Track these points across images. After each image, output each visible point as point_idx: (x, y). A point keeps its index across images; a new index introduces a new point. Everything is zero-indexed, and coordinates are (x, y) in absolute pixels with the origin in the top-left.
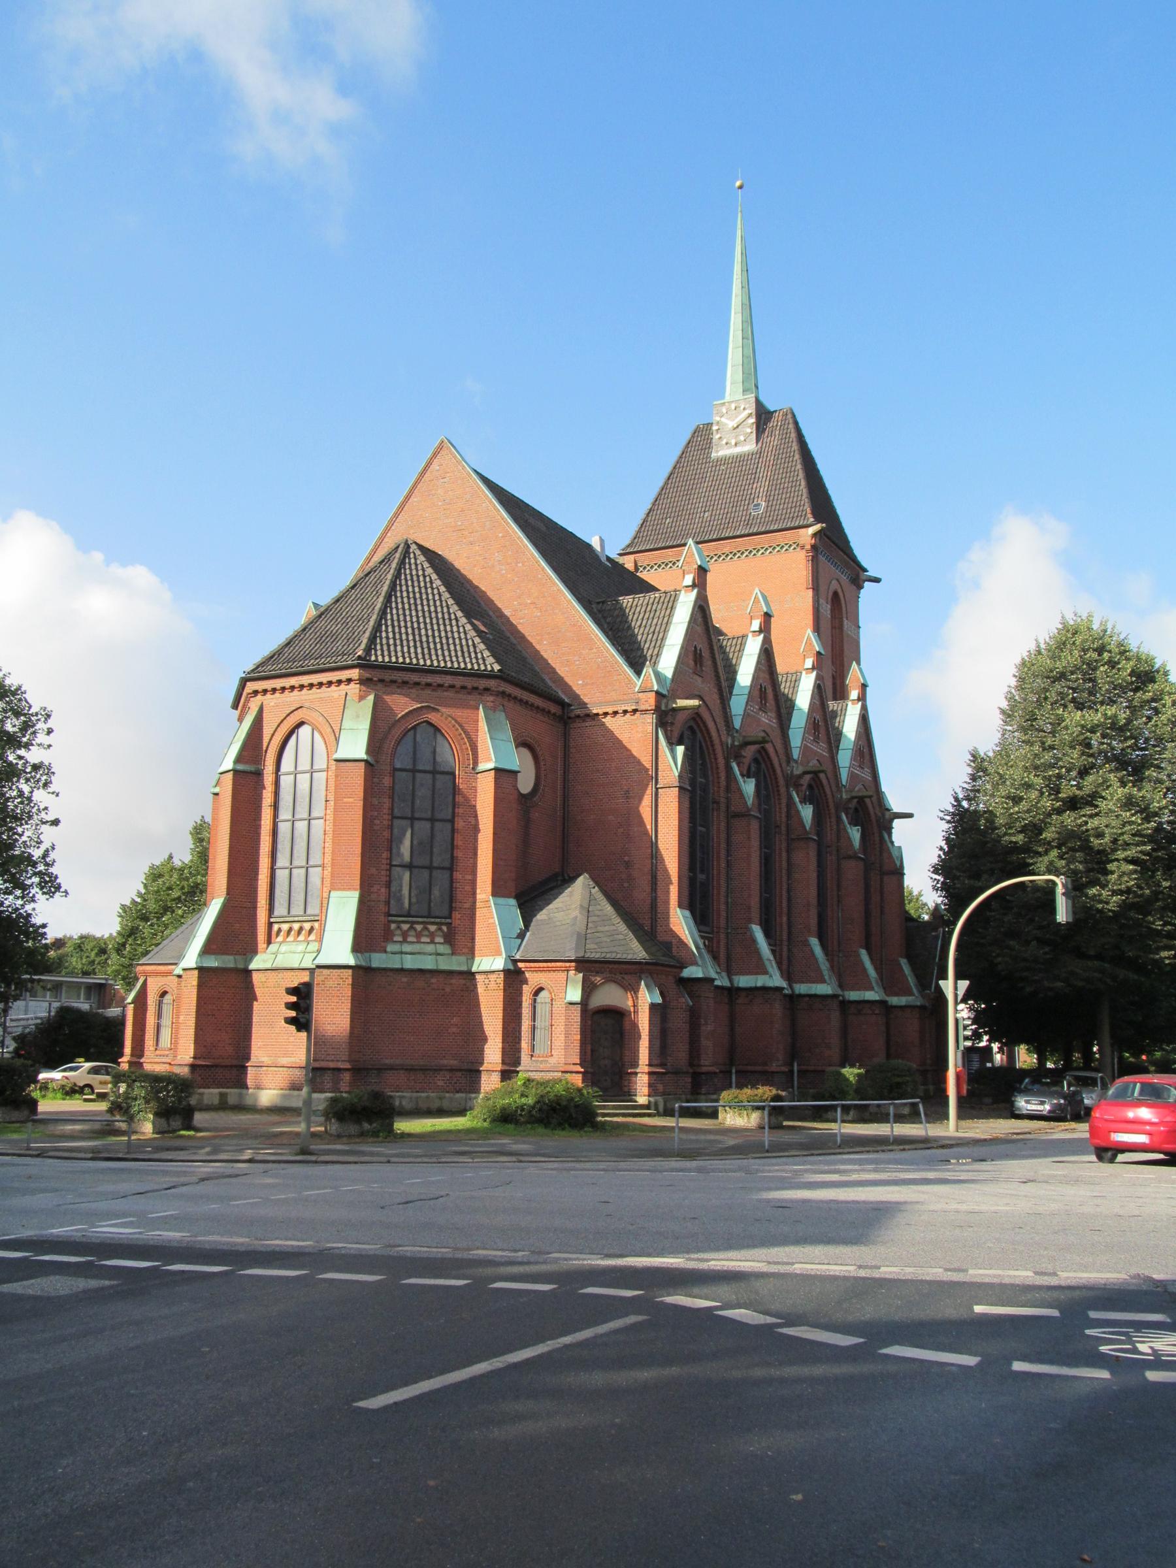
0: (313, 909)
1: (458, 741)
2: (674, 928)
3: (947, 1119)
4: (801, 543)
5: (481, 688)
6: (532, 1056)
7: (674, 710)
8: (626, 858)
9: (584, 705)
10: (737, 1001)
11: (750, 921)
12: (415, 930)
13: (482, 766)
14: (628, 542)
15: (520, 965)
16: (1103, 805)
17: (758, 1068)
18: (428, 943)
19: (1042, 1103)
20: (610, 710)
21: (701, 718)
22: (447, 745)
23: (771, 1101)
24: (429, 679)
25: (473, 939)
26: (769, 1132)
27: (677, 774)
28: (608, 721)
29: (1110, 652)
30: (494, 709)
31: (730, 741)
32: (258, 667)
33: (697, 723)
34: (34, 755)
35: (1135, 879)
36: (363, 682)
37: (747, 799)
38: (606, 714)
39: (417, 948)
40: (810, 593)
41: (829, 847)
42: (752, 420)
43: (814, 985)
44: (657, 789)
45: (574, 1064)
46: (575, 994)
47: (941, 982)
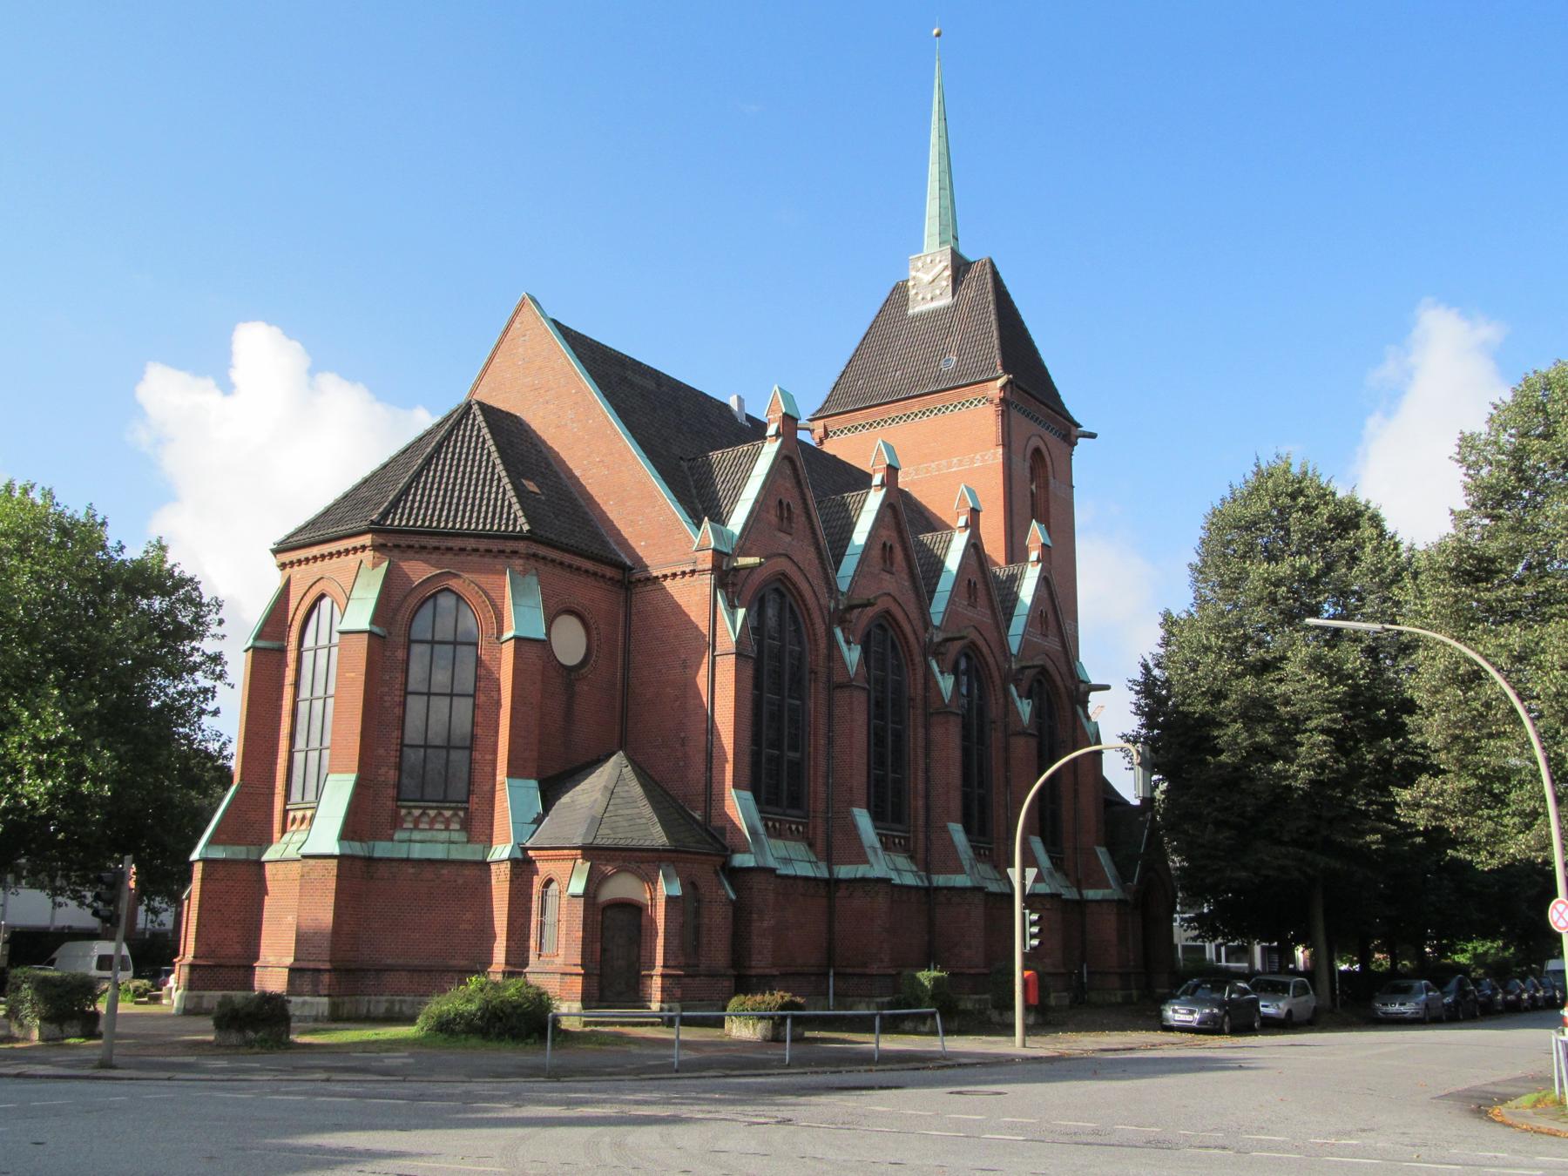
0: (310, 796)
1: (482, 609)
2: (728, 812)
4: (990, 397)
5: (417, 546)
6: (540, 955)
7: (735, 569)
8: (682, 735)
9: (645, 568)
10: (838, 894)
11: (851, 803)
12: (428, 815)
14: (819, 406)
15: (531, 853)
16: (1289, 668)
17: (858, 970)
18: (441, 830)
19: (1191, 1012)
20: (669, 572)
21: (789, 579)
22: (472, 615)
23: (778, 1009)
24: (451, 543)
25: (492, 825)
26: (790, 1045)
27: (734, 640)
28: (668, 584)
29: (1307, 496)
30: (525, 573)
31: (832, 605)
32: (288, 538)
33: (783, 583)
34: (208, 646)
35: (1327, 751)
37: (850, 668)
38: (665, 577)
39: (428, 835)
40: (1000, 450)
41: (994, 722)
42: (948, 273)
43: (953, 877)
44: (714, 657)
45: (575, 965)
46: (578, 886)
47: (1009, 870)
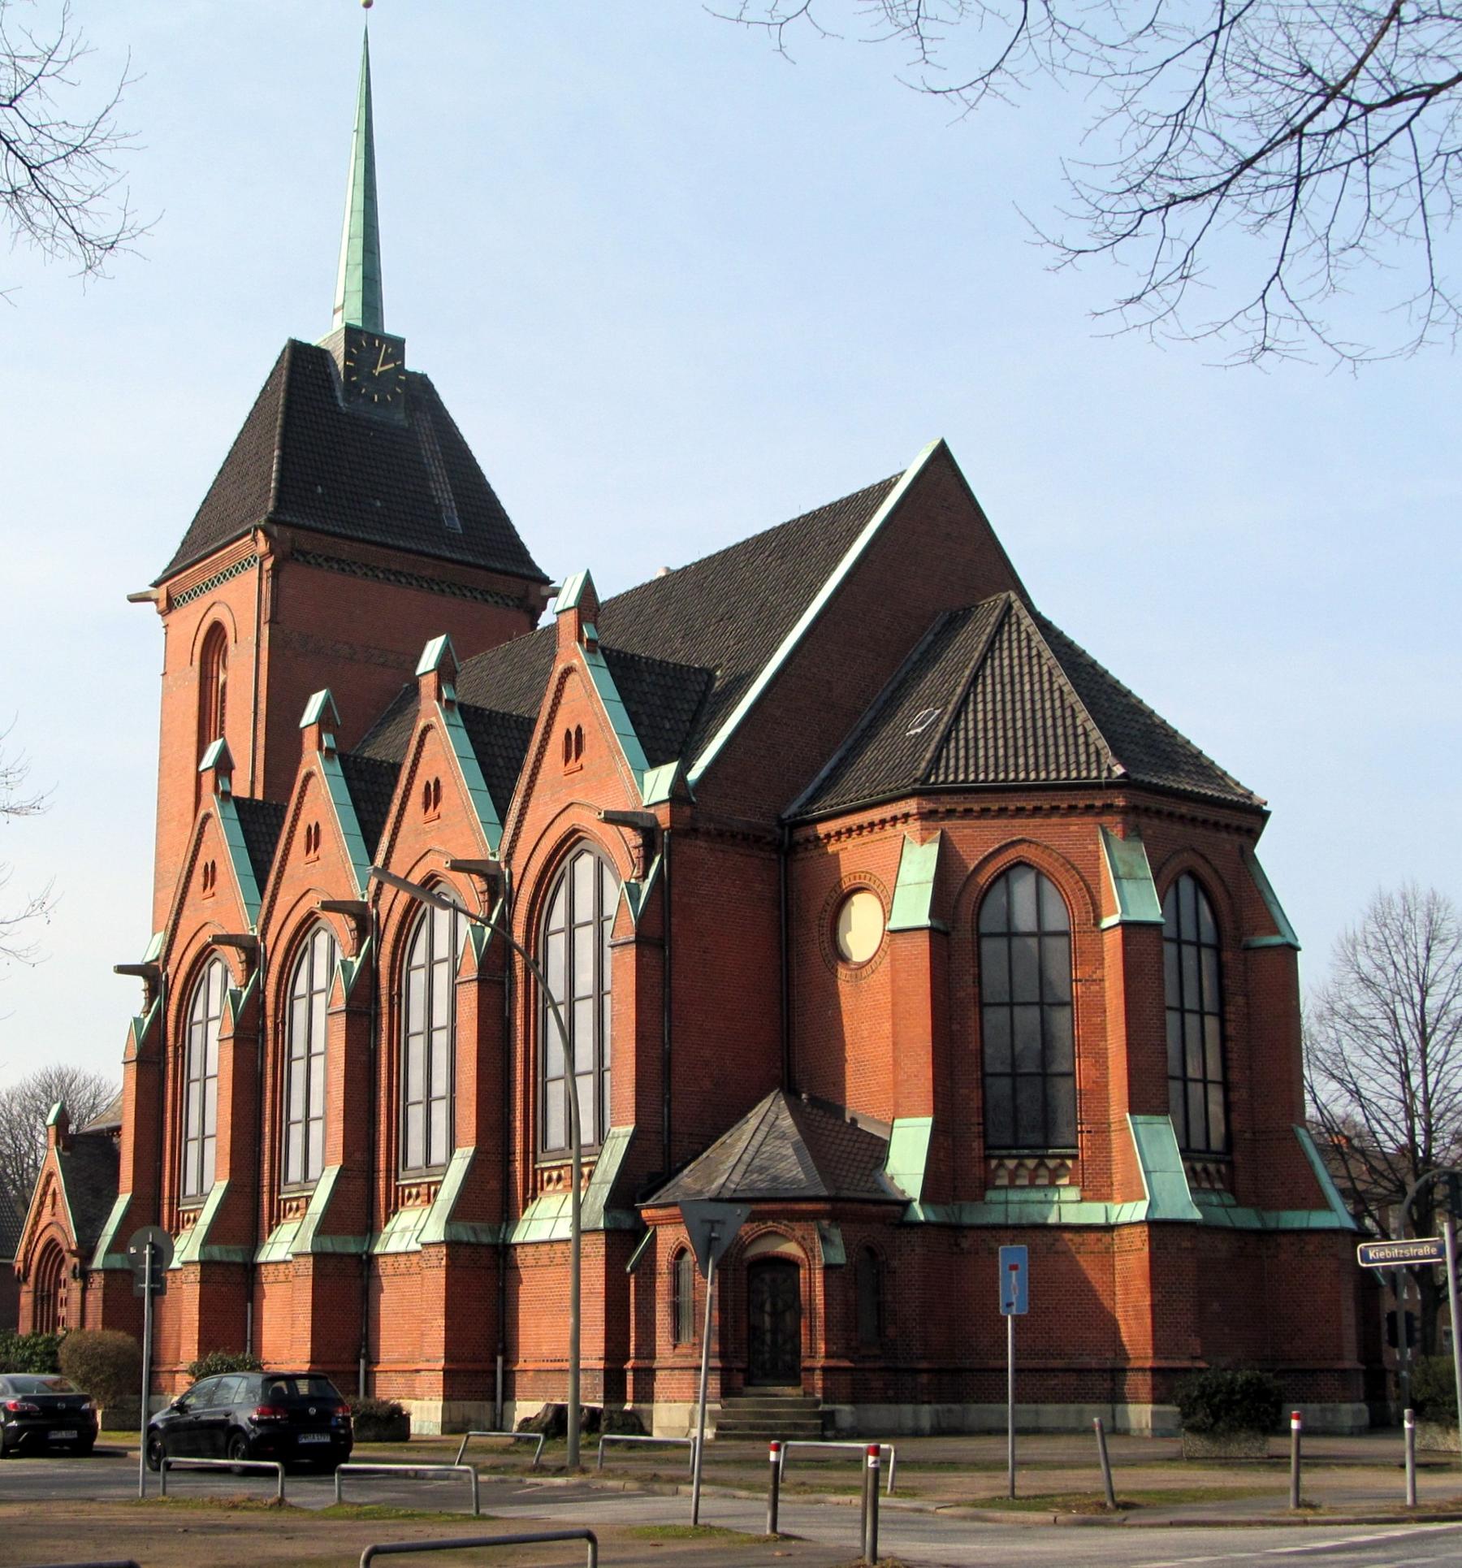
3: (1403, 1438)
6: (675, 1346)
13: (1106, 923)
36: (924, 816)
